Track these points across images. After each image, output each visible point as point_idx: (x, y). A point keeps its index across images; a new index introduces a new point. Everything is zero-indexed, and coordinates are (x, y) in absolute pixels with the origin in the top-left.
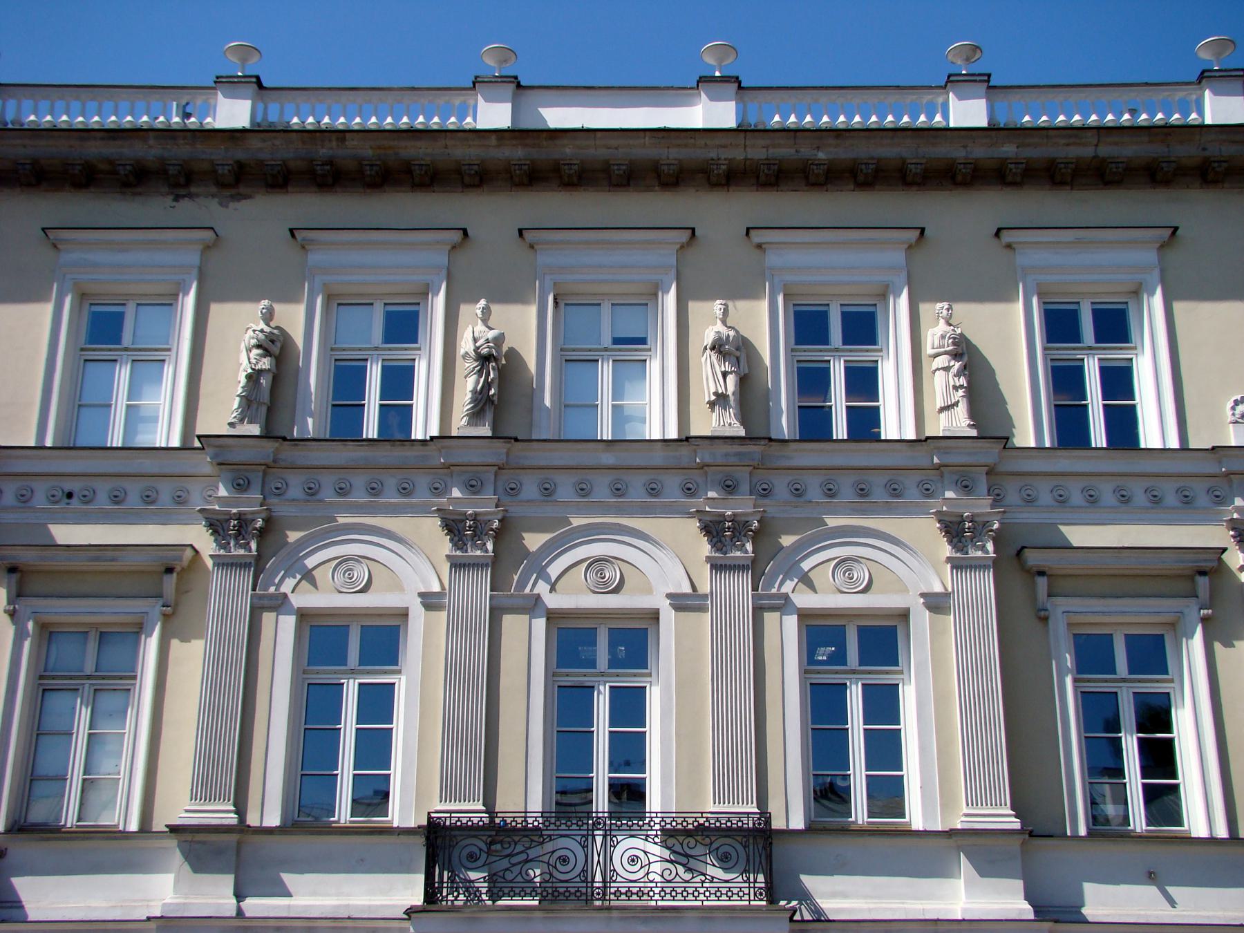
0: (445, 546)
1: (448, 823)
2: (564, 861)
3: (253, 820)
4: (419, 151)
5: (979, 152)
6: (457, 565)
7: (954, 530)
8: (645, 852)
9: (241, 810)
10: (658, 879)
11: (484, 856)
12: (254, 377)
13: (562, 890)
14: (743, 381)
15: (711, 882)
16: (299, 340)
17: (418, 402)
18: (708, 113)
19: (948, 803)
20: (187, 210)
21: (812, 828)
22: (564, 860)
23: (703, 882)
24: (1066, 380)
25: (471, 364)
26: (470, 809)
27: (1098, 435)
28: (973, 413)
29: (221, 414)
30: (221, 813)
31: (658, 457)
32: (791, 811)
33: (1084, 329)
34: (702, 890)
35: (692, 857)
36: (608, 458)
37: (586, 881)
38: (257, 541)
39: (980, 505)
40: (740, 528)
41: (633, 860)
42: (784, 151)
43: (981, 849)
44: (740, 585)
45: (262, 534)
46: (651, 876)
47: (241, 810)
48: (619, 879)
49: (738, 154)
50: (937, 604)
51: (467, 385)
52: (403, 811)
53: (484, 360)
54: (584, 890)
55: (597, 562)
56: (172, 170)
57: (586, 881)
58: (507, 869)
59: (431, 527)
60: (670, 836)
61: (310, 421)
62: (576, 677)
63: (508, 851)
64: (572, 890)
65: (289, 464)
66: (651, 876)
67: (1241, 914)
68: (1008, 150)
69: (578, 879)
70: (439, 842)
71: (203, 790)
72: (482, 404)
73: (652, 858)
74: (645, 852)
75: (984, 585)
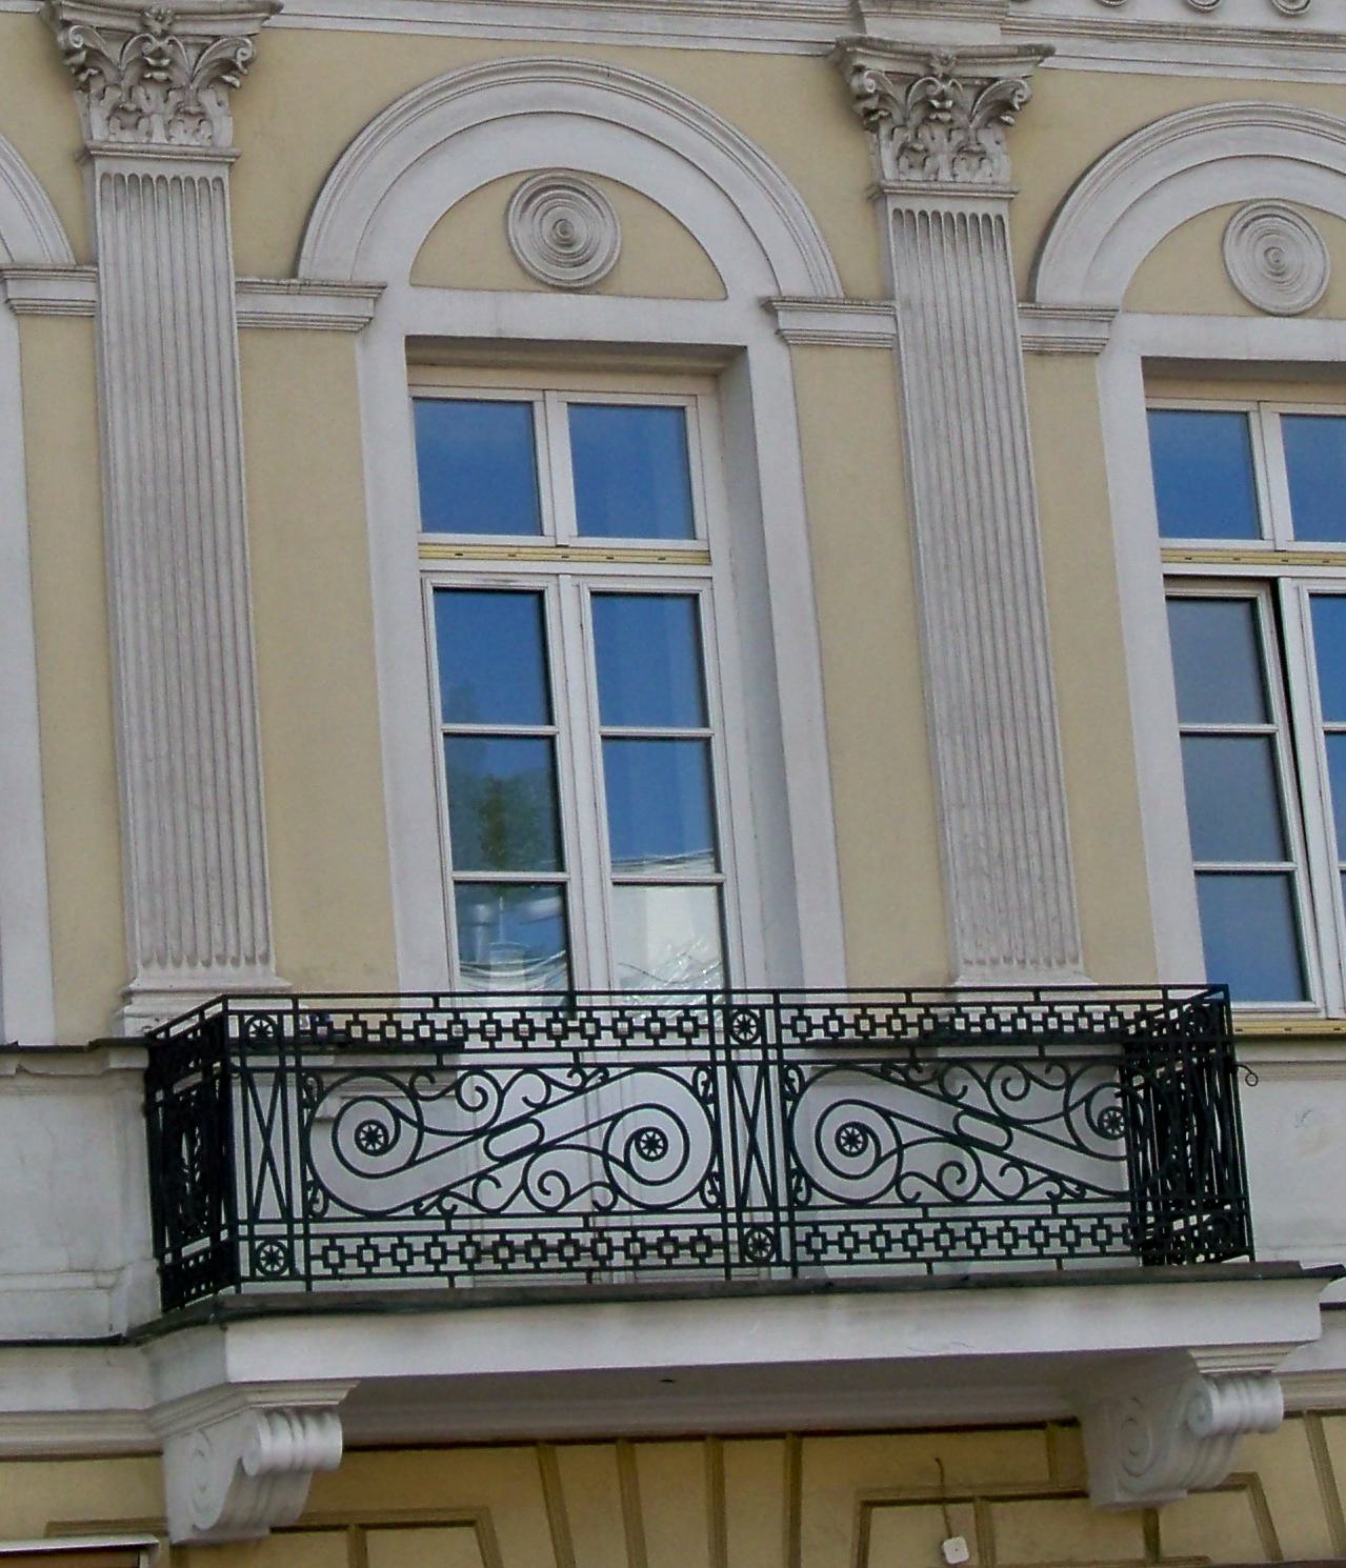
1: (289, 1030)
2: (372, 1137)
8: (1080, 1147)
9: (1121, 1158)
10: (930, 1194)
11: (409, 1133)
12: (1297, 1264)
13: (651, 1237)
15: (1079, 1198)
22: (650, 1143)
23: (1054, 1200)
34: (1054, 1226)
35: (1019, 1124)
37: (720, 1206)
41: (854, 1138)
46: (910, 1186)
47: (1121, 1158)
48: (818, 1199)
54: (716, 1235)
57: (720, 1206)
58: (482, 1175)
61: (1189, 1148)
63: (483, 1118)
64: (684, 1236)
66: (910, 1186)
69: (696, 1202)
73: (908, 1133)
74: (886, 1115)
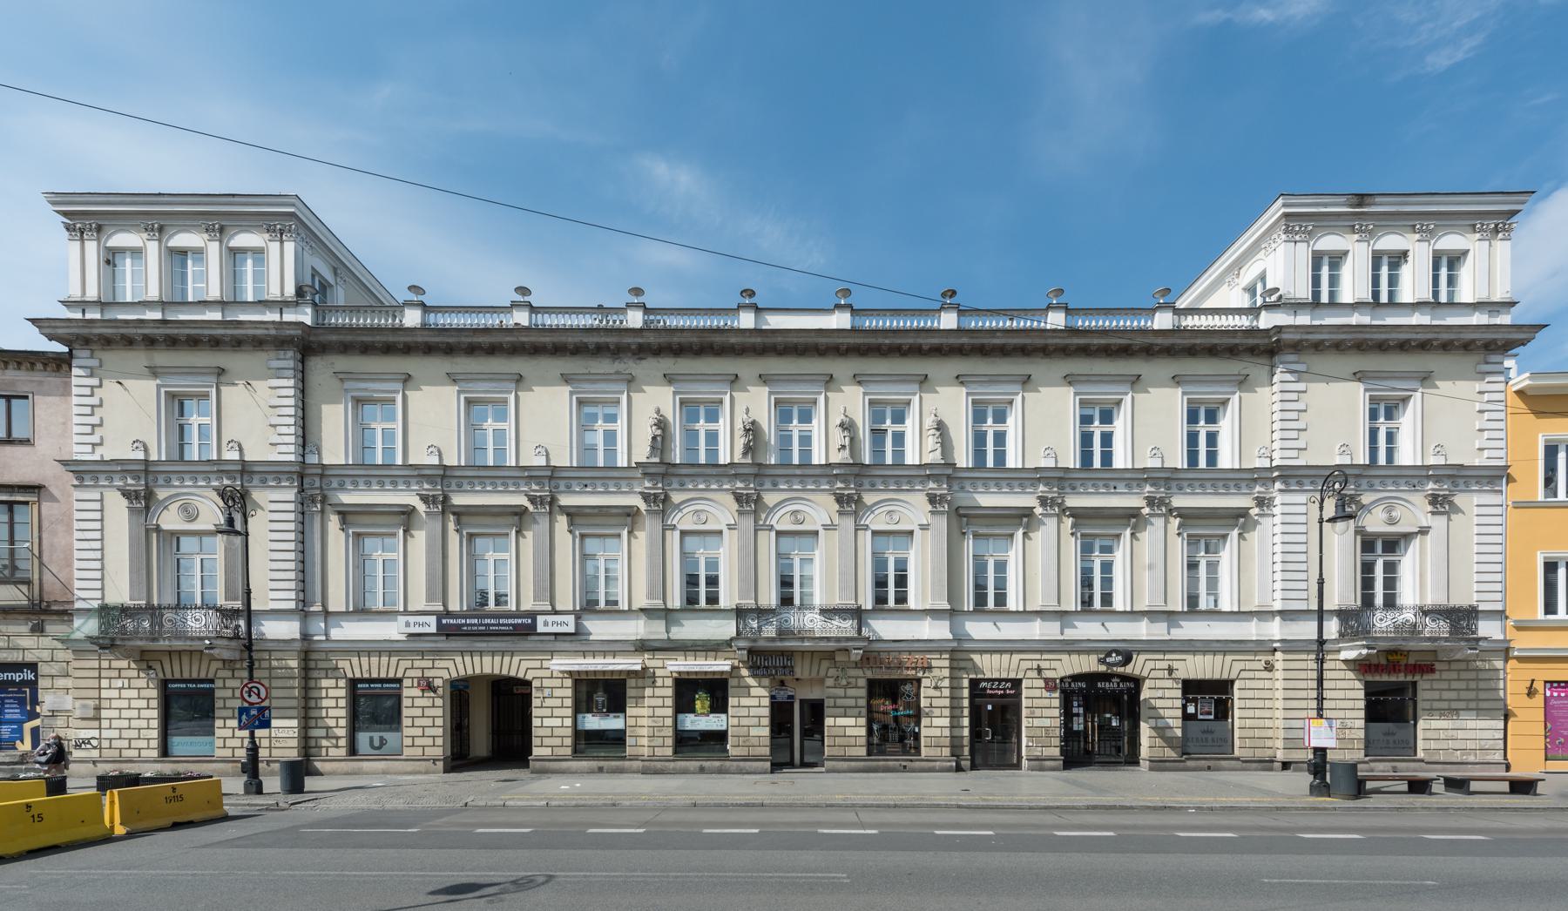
0: (736, 506)
3: (670, 606)
4: (717, 339)
5: (952, 341)
6: (740, 513)
7: (933, 499)
9: (445, 605)
14: (852, 439)
16: (671, 419)
17: (721, 447)
18: (839, 321)
19: (924, 599)
20: (618, 366)
21: (874, 610)
24: (980, 439)
25: (742, 432)
26: (749, 603)
27: (1097, 463)
28: (943, 453)
29: (642, 453)
30: (658, 603)
31: (818, 472)
32: (868, 604)
33: (1203, 413)
36: (798, 472)
38: (661, 504)
39: (943, 490)
40: (850, 498)
42: (871, 340)
43: (934, 613)
44: (849, 523)
45: (664, 501)
47: (445, 605)
49: (851, 341)
50: (924, 527)
51: (740, 443)
52: (724, 603)
53: (747, 431)
55: (794, 512)
56: (39, 366)
59: (730, 499)
60: (823, 612)
62: (1369, 557)
65: (665, 474)
67: (3, 628)
68: (965, 340)
70: (740, 613)
71: (651, 595)
72: (748, 449)
75: (942, 522)
